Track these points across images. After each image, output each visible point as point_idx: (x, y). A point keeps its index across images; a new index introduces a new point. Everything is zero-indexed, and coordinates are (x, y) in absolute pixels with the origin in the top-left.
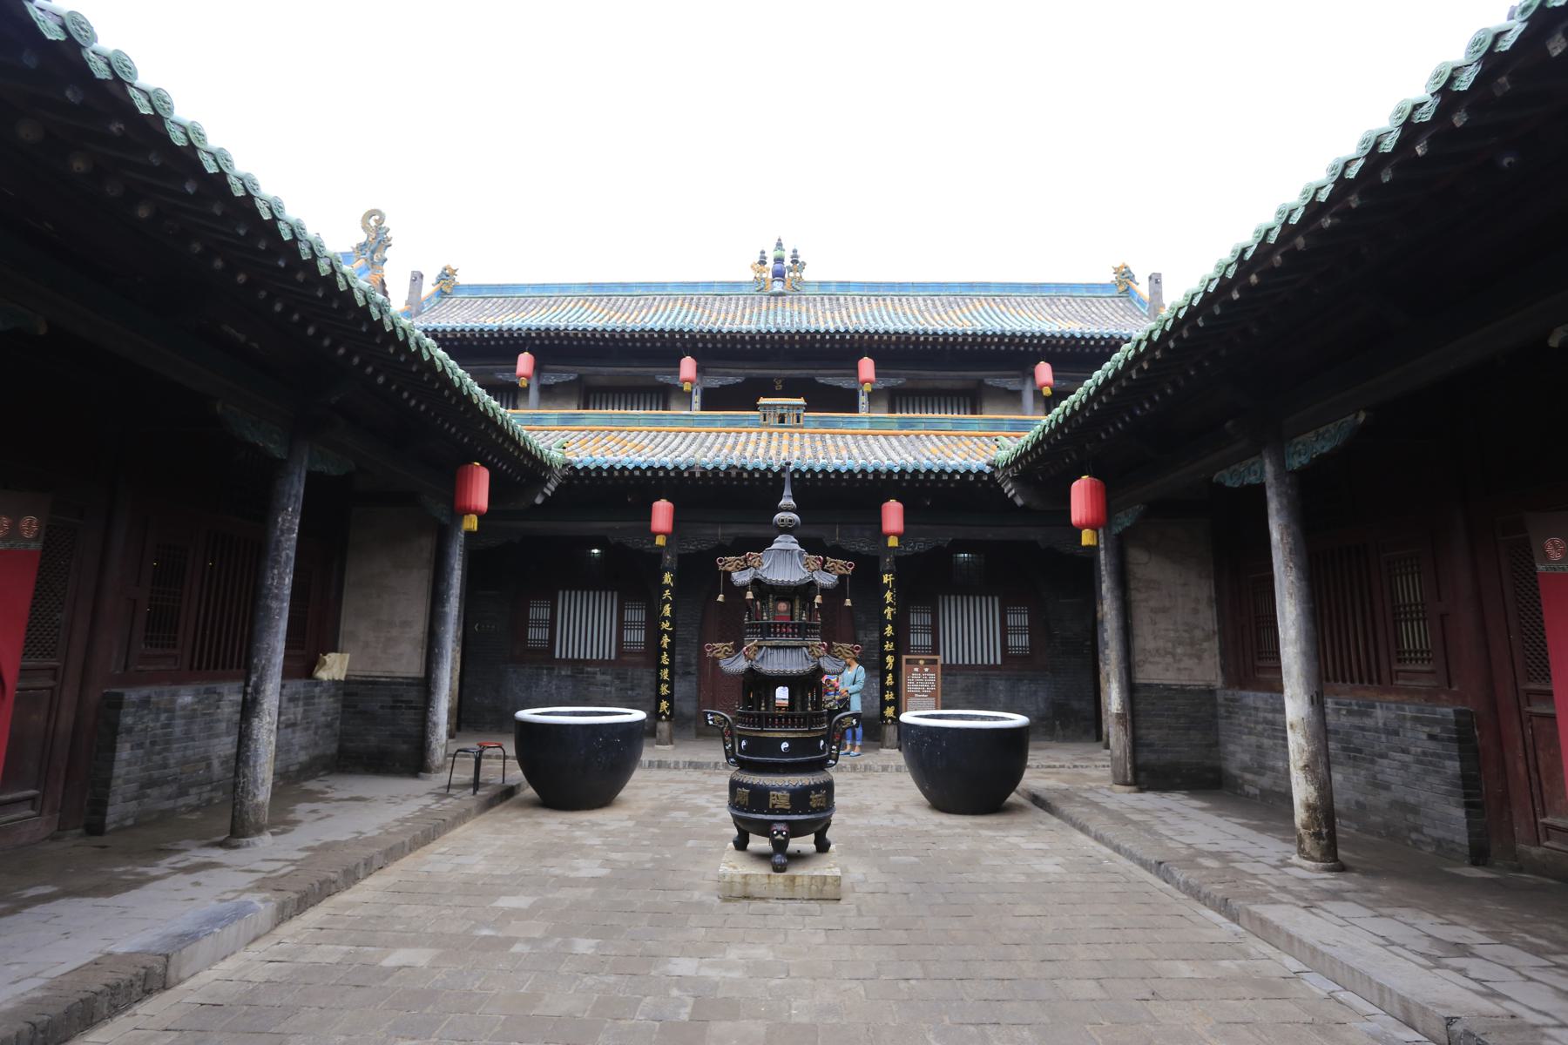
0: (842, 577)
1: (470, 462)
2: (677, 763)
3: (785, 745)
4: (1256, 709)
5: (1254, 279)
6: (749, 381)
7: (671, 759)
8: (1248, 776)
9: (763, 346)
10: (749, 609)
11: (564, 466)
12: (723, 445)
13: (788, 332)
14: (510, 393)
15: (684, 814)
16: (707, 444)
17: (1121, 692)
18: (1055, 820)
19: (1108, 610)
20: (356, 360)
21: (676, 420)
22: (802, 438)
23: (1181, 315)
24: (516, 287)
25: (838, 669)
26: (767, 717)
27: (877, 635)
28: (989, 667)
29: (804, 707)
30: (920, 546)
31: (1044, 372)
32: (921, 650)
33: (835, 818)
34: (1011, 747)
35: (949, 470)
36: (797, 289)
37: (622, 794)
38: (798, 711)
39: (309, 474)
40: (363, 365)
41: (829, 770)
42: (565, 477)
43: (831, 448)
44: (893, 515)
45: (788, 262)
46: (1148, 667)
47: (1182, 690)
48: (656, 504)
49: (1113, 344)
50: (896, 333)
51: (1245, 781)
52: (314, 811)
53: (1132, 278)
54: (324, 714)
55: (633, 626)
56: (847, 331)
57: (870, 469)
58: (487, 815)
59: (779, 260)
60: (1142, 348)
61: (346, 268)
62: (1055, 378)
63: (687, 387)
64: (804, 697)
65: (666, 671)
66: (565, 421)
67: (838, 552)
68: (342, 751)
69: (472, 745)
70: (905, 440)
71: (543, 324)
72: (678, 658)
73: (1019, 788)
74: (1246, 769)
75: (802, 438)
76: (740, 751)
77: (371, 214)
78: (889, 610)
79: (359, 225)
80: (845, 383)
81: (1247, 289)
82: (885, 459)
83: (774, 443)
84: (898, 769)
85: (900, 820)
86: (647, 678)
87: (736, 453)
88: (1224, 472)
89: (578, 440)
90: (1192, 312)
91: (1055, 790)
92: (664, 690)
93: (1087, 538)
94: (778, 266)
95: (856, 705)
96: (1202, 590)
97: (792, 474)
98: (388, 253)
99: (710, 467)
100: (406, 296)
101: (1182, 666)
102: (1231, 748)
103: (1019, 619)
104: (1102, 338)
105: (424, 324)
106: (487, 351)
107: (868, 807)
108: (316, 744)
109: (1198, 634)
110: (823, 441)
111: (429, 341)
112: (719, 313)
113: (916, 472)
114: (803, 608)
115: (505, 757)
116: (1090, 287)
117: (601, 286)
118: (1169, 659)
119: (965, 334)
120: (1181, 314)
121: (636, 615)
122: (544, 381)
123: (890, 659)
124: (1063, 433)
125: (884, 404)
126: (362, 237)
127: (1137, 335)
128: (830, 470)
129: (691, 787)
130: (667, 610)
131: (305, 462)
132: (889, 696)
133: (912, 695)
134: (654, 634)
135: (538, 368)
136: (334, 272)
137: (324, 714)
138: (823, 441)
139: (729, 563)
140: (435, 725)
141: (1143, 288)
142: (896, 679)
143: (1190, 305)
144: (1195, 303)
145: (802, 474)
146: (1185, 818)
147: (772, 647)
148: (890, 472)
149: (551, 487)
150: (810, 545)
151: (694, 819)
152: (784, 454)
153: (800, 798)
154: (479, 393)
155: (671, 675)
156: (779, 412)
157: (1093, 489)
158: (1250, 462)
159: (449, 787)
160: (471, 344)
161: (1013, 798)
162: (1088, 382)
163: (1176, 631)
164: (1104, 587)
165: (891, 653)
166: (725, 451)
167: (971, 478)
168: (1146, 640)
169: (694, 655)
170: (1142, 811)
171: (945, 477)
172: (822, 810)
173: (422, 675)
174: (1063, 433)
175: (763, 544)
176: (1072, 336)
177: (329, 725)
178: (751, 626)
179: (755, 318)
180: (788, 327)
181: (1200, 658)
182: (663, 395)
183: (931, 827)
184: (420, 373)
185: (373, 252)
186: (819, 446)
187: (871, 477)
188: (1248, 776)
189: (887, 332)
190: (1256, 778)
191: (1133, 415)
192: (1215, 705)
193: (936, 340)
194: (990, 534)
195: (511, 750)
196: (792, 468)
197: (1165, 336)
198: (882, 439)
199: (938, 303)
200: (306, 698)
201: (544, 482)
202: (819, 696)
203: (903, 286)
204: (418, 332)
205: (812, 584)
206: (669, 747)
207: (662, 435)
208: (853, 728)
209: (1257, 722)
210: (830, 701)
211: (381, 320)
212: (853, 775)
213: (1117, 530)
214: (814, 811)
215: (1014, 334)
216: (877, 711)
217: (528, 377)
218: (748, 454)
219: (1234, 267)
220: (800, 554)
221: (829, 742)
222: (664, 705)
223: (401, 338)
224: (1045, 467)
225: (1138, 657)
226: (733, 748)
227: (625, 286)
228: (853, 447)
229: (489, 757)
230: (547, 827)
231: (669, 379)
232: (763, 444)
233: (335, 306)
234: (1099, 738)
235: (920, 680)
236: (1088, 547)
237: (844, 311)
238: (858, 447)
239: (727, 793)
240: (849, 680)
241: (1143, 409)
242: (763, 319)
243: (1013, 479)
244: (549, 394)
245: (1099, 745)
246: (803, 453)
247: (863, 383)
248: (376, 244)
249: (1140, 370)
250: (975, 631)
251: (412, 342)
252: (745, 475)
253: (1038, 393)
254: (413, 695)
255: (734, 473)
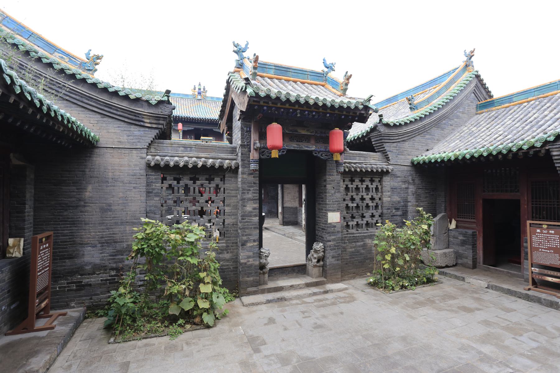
45: (202, 90)
47: (292, 208)
59: (200, 89)
168: (286, 199)
225: (284, 202)
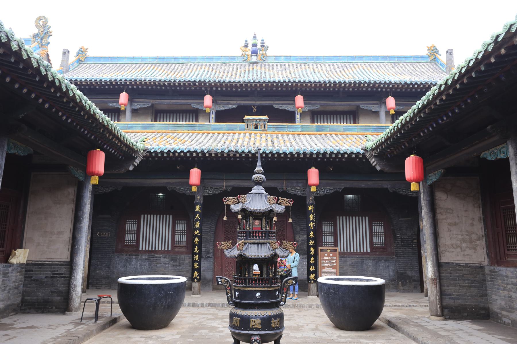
0: (287, 207)
1: (94, 147)
2: (202, 304)
3: (258, 294)
4: (507, 277)
5: (503, 51)
6: (240, 107)
7: (199, 302)
8: (504, 313)
9: (246, 89)
10: (240, 224)
11: (144, 151)
12: (226, 140)
13: (259, 82)
14: (116, 113)
15: (206, 331)
16: (218, 139)
17: (433, 267)
18: (400, 335)
19: (426, 224)
20: (33, 96)
21: (202, 126)
22: (266, 136)
23: (463, 71)
24: (119, 58)
25: (286, 255)
26: (249, 280)
27: (305, 237)
28: (364, 254)
29: (268, 275)
30: (328, 192)
31: (391, 102)
32: (328, 244)
33: (285, 332)
34: (376, 295)
35: (342, 152)
36: (264, 60)
37: (174, 321)
38: (265, 276)
39: (8, 155)
40: (37, 98)
41: (281, 307)
42: (144, 157)
43: (282, 141)
44: (313, 175)
45: (259, 46)
46: (447, 254)
47: (466, 266)
48: (192, 170)
49: (427, 87)
50: (315, 82)
51: (503, 316)
52: (6, 335)
53: (437, 52)
54: (14, 282)
55: (180, 233)
56: (289, 82)
57: (301, 152)
58: (102, 333)
60: (442, 88)
61: (26, 47)
62: (396, 104)
63: (208, 110)
64: (268, 270)
65: (197, 256)
66: (145, 128)
67: (285, 194)
68: (23, 301)
69: (94, 296)
70: (319, 137)
71: (133, 78)
72: (203, 249)
73: (380, 317)
74: (503, 309)
75: (266, 136)
76: (235, 297)
77: (40, 18)
78: (311, 224)
79: (34, 24)
80: (289, 108)
81: (499, 57)
82: (309, 147)
83: (252, 139)
84: (317, 307)
85: (318, 334)
86: (187, 259)
87: (233, 144)
88: (487, 152)
89: (149, 137)
90: (469, 70)
91: (400, 318)
92: (196, 266)
93: (414, 187)
94: (254, 48)
95: (295, 273)
96: (477, 213)
97: (261, 155)
98: (50, 40)
99: (219, 151)
100: (60, 62)
101: (466, 253)
102: (494, 297)
103: (379, 228)
104: (421, 83)
105: (71, 77)
106: (104, 91)
107: (302, 327)
108: (9, 298)
109: (474, 237)
110: (277, 137)
111: (73, 86)
112: (224, 73)
113: (325, 153)
114: (267, 223)
115: (112, 302)
116: (415, 57)
117: (163, 58)
118: (459, 250)
119: (350, 83)
120: (463, 71)
121: (182, 227)
122: (134, 107)
123: (312, 249)
124: (401, 133)
125: (309, 118)
126: (36, 31)
127: (439, 83)
128: (281, 152)
129: (210, 316)
130: (198, 224)
131: (6, 147)
132: (312, 269)
133: (324, 268)
134: (191, 236)
135: (131, 100)
136: (20, 49)
137: (14, 282)
138: (277, 137)
139: (229, 200)
140: (75, 286)
141: (443, 58)
142: (316, 259)
143: (468, 66)
144: (471, 64)
145: (267, 155)
146: (470, 335)
147: (252, 243)
148: (312, 154)
149: (137, 162)
150: (271, 191)
151: (212, 334)
152: (257, 144)
153: (266, 322)
154: (100, 114)
155: (200, 258)
156: (255, 123)
157: (416, 162)
158: (501, 147)
159: (81, 319)
160: (95, 87)
161: (377, 322)
162: (414, 107)
163: (462, 235)
164: (423, 212)
165: (313, 246)
166: (227, 143)
167: (353, 156)
168: (445, 239)
169: (212, 247)
170: (447, 331)
171: (340, 156)
172: (277, 328)
173: (68, 260)
174: (401, 133)
175: (246, 190)
176: (406, 83)
177: (16, 288)
178: (241, 233)
179: (242, 75)
180: (259, 79)
181: (475, 249)
182: (195, 114)
183: (335, 338)
184: (68, 102)
185: (42, 39)
186: (275, 140)
187: (302, 156)
188: (504, 313)
189: (310, 82)
190: (509, 314)
191: (437, 123)
192: (484, 275)
193: (335, 86)
194: (363, 185)
195: (115, 299)
196: (261, 152)
197: (454, 82)
198: (307, 136)
199: (336, 67)
200: (4, 274)
201: (134, 159)
202: (276, 267)
203: (318, 58)
204: (66, 81)
205: (271, 211)
206: (199, 296)
207: (195, 135)
208: (294, 285)
209: (508, 284)
210: (281, 271)
211: (46, 75)
212: (294, 310)
213: (429, 182)
214: (273, 329)
215: (375, 82)
216: (306, 276)
217: (125, 105)
218: (239, 145)
219: (492, 45)
220: (266, 196)
221: (280, 292)
222: (196, 273)
223: (57, 84)
224: (392, 151)
225: (441, 249)
226: (231, 296)
227: (175, 58)
228: (292, 140)
229: (104, 302)
230: (133, 340)
231: (198, 106)
232: (247, 139)
233: (21, 67)
234: (422, 291)
235: (327, 260)
236: (415, 191)
237: (288, 71)
238: (295, 140)
239: (228, 320)
240: (292, 261)
241: (442, 120)
242: (246, 75)
243: (375, 157)
244: (136, 113)
245: (423, 294)
246: (267, 144)
247: (298, 108)
248: (43, 35)
249: (441, 100)
250: (356, 234)
251: (63, 86)
252: (238, 155)
253: (387, 112)
254: (63, 270)
255: (232, 155)
